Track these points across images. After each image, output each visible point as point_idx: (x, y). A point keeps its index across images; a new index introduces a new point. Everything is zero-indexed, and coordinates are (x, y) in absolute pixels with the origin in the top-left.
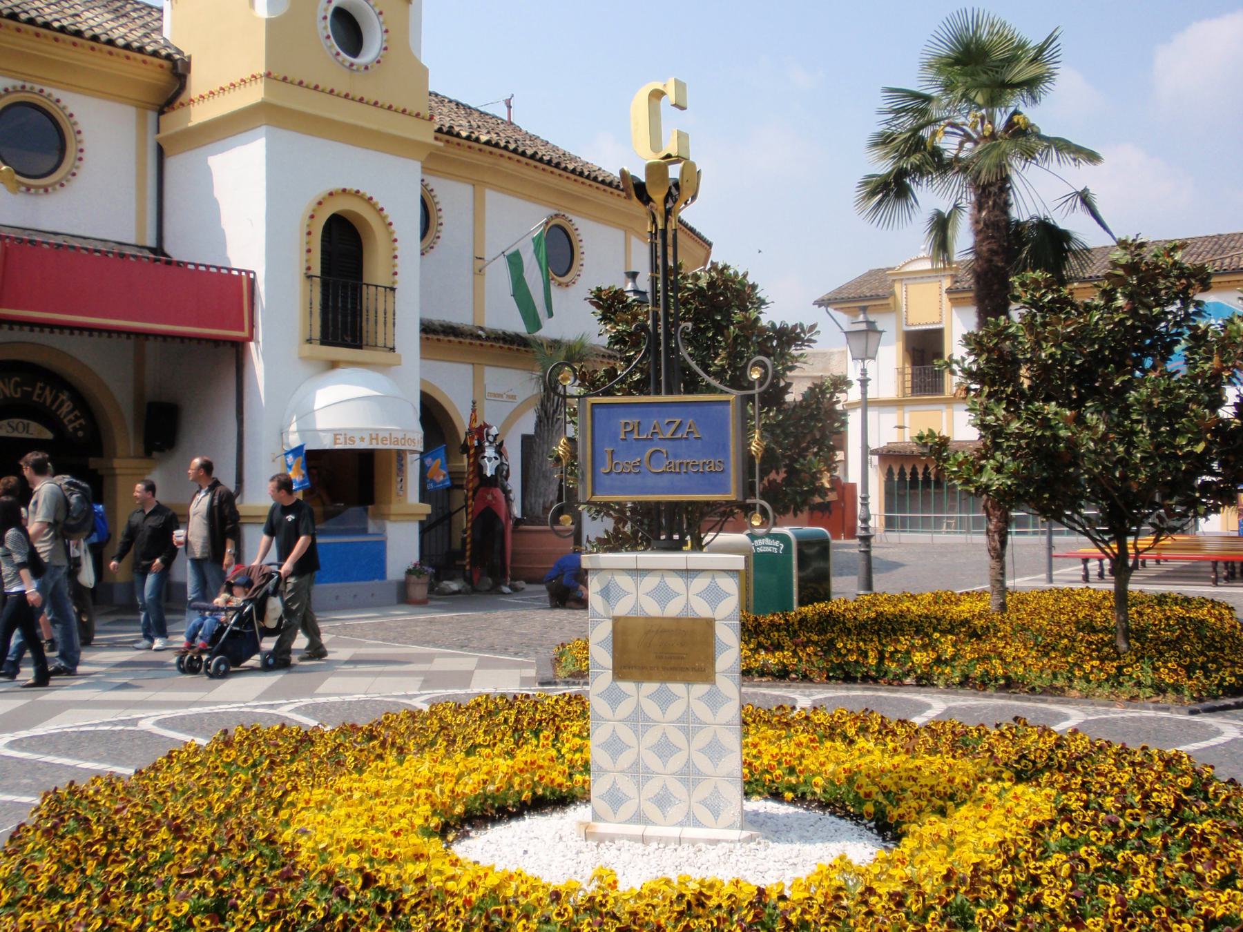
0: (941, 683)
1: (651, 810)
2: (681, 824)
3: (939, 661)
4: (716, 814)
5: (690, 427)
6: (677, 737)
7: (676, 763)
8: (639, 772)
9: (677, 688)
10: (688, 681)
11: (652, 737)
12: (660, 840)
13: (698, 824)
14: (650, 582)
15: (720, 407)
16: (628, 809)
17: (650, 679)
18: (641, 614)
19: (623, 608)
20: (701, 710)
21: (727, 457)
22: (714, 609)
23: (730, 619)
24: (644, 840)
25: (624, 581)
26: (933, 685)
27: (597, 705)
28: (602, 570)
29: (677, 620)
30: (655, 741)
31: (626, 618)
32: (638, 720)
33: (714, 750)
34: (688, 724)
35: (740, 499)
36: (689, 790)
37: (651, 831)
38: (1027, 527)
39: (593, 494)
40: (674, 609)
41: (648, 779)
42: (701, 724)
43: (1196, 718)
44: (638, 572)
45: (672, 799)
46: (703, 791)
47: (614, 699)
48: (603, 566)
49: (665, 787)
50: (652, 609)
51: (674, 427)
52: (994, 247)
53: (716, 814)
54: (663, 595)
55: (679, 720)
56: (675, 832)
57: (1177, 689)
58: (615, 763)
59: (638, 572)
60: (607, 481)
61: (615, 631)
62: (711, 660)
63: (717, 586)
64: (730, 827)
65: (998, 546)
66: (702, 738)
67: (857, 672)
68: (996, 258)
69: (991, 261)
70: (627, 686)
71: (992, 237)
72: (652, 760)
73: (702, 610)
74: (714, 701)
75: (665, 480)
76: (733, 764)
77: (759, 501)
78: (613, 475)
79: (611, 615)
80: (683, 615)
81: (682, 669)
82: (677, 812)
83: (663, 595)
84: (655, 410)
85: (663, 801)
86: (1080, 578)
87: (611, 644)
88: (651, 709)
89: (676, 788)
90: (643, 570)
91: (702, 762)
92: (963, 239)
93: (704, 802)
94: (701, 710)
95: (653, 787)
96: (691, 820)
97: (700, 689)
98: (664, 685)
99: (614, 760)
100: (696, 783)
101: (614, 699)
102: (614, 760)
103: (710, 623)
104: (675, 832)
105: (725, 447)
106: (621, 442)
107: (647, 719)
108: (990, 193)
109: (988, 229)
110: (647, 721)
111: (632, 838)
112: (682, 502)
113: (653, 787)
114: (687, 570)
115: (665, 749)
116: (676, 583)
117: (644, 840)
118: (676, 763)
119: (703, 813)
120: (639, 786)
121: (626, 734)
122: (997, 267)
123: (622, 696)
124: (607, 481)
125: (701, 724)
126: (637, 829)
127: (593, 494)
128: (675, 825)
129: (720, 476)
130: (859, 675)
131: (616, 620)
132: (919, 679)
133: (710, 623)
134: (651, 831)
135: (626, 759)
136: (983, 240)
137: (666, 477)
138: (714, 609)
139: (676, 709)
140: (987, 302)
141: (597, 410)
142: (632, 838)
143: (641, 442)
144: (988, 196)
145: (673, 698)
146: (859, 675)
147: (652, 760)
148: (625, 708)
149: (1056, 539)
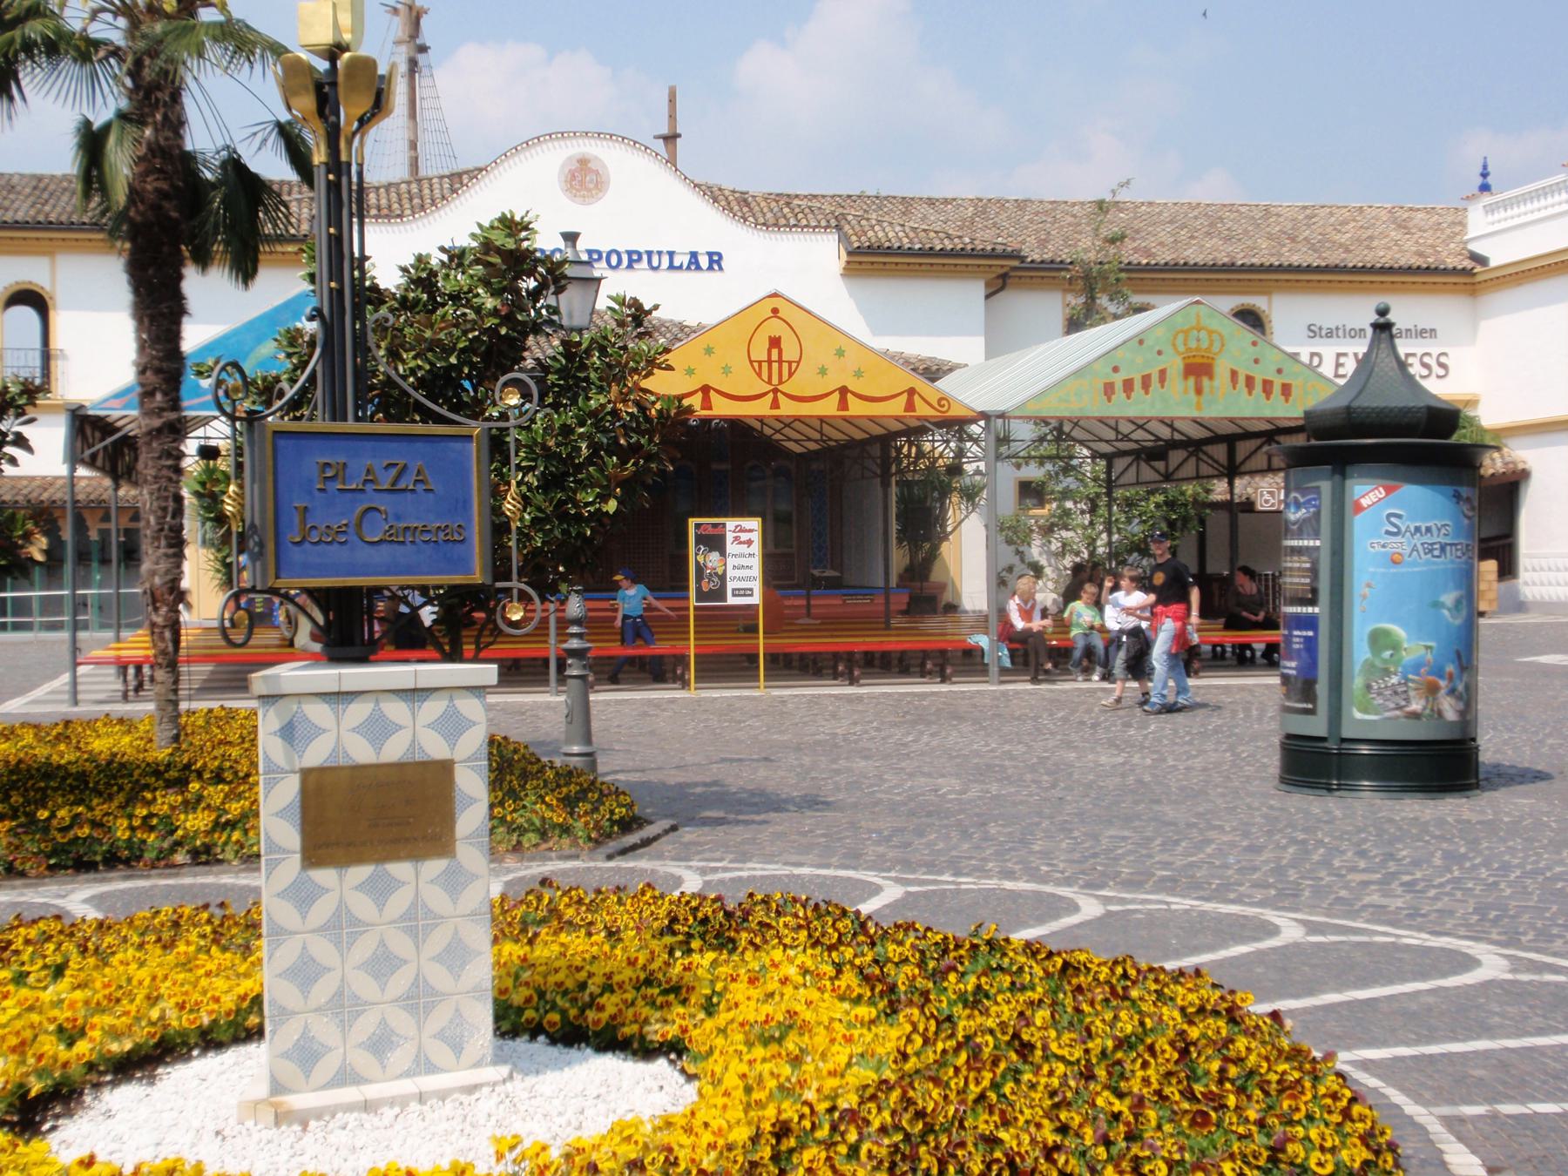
0: (229, 854)
1: (362, 1061)
2: (408, 1074)
3: (218, 826)
4: (457, 1048)
5: (419, 473)
6: (401, 944)
7: (400, 982)
8: (344, 1007)
9: (400, 869)
10: (417, 856)
11: (364, 948)
12: (391, 1102)
13: (432, 1069)
14: (358, 711)
15: (458, 445)
16: (327, 1066)
17: (360, 860)
18: (342, 762)
19: (316, 754)
20: (437, 898)
21: (469, 520)
22: (453, 746)
23: (476, 759)
24: (368, 1107)
25: (318, 712)
26: (220, 862)
27: (275, 910)
28: (283, 696)
29: (399, 766)
30: (368, 954)
31: (321, 770)
32: (342, 927)
33: (455, 956)
34: (417, 922)
35: (489, 582)
36: (418, 1022)
37: (371, 1091)
38: (30, 614)
39: (277, 577)
40: (394, 750)
41: (359, 1014)
42: (436, 919)
43: (611, 864)
44: (415, 694)
45: (394, 1039)
46: (440, 1018)
47: (303, 897)
48: (286, 689)
49: (383, 1022)
50: (362, 752)
51: (394, 472)
52: (164, 186)
53: (457, 1048)
54: (378, 729)
55: (403, 918)
56: (407, 1086)
57: (566, 830)
58: (306, 998)
59: (415, 694)
60: (296, 555)
61: (304, 791)
62: (446, 819)
63: (457, 713)
64: (478, 1064)
65: (171, 648)
66: (437, 941)
67: (95, 853)
68: (166, 204)
69: (160, 207)
70: (324, 876)
71: (161, 171)
72: (365, 986)
73: (436, 748)
74: (454, 883)
75: (384, 554)
76: (481, 973)
77: (515, 584)
78: (307, 546)
79: (297, 766)
80: (408, 758)
81: (407, 840)
82: (400, 1057)
83: (378, 729)
84: (369, 445)
85: (380, 1044)
86: (66, 697)
87: (298, 811)
88: (362, 906)
89: (401, 1021)
90: (347, 693)
91: (438, 977)
92: (121, 163)
93: (440, 1035)
94: (437, 898)
95: (366, 1025)
96: (423, 1065)
97: (434, 867)
98: (380, 868)
99: (305, 993)
100: (429, 1008)
101: (303, 897)
102: (305, 993)
103: (444, 770)
104: (407, 1086)
105: (466, 504)
106: (317, 494)
107: (355, 922)
108: (157, 100)
109: (154, 157)
110: (355, 925)
111: (349, 1108)
112: (361, 588)
113: (366, 1025)
114: (414, 690)
115: (383, 964)
116: (396, 710)
117: (368, 1107)
118: (400, 982)
119: (439, 1052)
120: (345, 1027)
121: (323, 950)
122: (170, 218)
123: (316, 893)
124: (296, 555)
125: (436, 919)
126: (350, 1094)
127: (277, 577)
128: (400, 1077)
129: (461, 547)
130: (98, 858)
131: (306, 773)
132: (195, 854)
133: (444, 770)
134: (371, 1091)
135: (322, 991)
136: (146, 173)
137: (384, 548)
138: (453, 746)
139: (399, 902)
140: (151, 272)
141: (282, 443)
142: (349, 1108)
143: (349, 495)
144: (155, 106)
145: (394, 884)
146: (98, 858)
147: (365, 986)
148: (322, 910)
149: (82, 635)
